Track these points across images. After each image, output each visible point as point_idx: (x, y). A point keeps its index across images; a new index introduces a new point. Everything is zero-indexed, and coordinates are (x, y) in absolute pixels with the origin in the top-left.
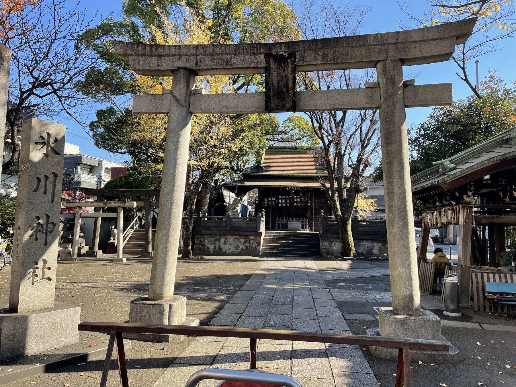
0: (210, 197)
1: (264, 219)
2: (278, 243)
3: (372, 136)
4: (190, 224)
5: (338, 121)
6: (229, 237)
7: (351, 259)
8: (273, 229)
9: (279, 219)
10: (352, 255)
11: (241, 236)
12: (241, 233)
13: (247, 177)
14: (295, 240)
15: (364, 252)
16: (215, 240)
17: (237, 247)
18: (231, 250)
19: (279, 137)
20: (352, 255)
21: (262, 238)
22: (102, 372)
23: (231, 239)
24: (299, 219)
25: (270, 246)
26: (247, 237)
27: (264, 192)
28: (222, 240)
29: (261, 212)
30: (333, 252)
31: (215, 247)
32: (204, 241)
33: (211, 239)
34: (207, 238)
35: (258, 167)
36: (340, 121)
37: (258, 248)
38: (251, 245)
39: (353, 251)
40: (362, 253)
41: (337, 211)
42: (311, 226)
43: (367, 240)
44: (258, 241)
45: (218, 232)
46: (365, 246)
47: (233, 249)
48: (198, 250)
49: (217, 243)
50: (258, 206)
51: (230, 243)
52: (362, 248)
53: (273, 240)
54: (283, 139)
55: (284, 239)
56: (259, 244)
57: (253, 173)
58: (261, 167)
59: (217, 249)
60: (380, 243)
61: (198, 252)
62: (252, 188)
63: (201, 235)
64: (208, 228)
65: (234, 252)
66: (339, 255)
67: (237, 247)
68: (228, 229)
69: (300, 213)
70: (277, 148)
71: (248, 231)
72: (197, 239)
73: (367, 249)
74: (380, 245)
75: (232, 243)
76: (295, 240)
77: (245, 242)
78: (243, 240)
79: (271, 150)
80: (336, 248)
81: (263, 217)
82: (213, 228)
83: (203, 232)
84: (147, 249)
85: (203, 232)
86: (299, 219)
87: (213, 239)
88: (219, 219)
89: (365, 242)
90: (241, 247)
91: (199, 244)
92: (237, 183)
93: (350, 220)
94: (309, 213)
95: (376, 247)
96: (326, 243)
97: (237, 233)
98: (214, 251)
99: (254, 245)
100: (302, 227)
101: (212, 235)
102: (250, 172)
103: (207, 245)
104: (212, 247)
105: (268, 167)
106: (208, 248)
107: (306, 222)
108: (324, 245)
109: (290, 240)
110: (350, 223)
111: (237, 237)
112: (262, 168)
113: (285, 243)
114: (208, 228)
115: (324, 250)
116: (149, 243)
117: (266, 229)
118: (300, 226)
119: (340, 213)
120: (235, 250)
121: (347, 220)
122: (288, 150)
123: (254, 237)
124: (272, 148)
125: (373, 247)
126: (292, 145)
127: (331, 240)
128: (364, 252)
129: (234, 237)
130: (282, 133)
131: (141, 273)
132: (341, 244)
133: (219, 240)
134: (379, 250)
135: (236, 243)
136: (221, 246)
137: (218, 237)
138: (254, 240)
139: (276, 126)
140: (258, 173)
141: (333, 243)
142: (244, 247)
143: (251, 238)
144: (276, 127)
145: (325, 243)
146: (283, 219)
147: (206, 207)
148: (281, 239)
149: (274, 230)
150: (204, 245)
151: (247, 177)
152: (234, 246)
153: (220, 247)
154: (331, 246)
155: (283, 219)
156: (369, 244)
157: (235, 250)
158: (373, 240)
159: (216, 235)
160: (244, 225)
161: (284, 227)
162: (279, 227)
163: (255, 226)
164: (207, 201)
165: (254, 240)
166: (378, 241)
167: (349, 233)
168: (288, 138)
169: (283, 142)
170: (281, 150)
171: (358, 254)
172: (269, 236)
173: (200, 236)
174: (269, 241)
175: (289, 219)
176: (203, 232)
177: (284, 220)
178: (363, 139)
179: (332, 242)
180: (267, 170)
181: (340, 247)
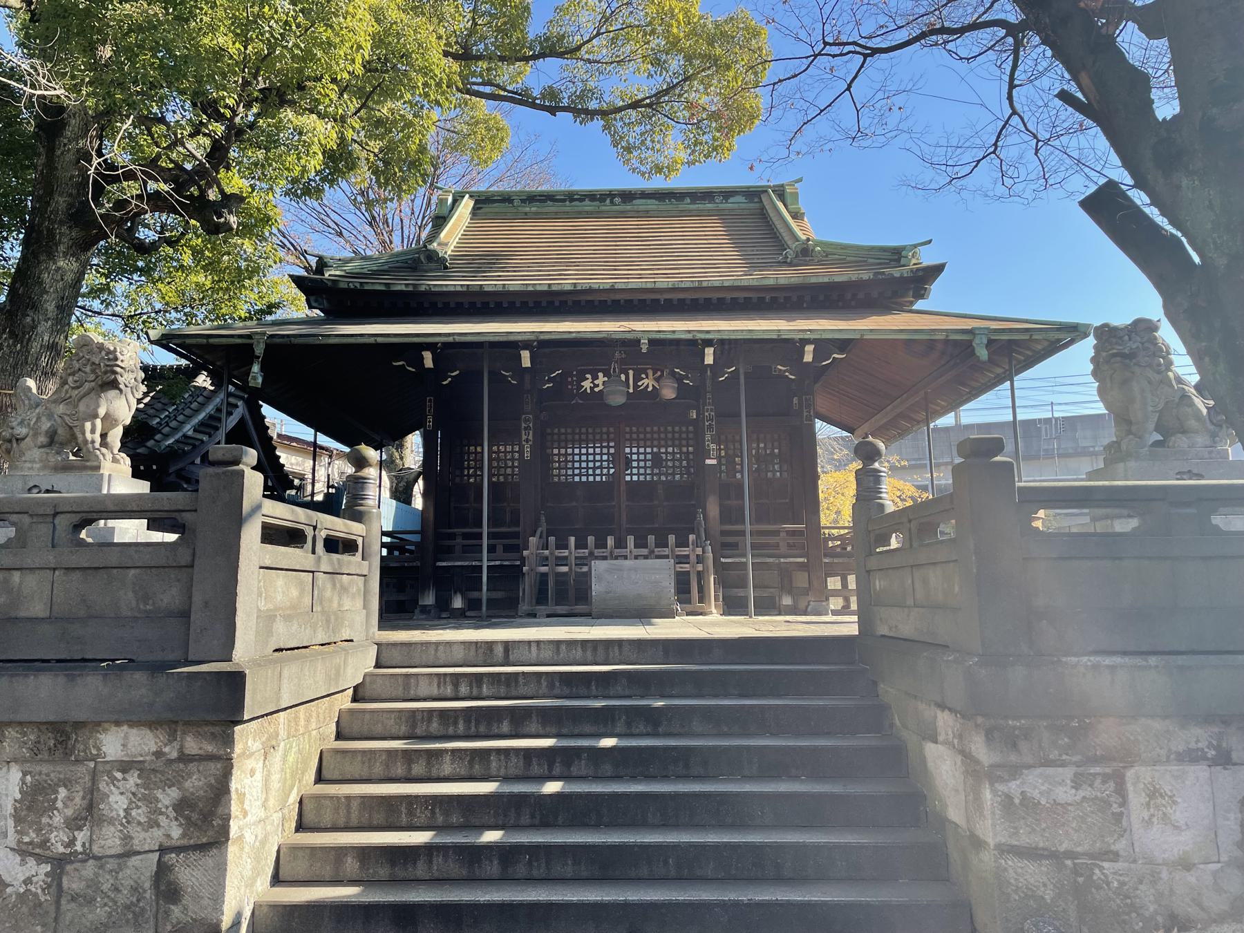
2: (477, 765)
22: (819, 424)
24: (662, 543)
25: (390, 813)
37: (188, 874)
38: (110, 840)
54: (551, 93)
56: (207, 822)
86: (662, 543)
94: (713, 509)
100: (683, 587)
107: (700, 559)
115: (1032, 875)
118: (669, 586)
122: (588, 206)
130: (552, 48)
131: (783, 534)
143: (113, 744)
145: (1034, 784)
146: (682, 543)
161: (571, 599)
170: (551, 207)
175: (601, 544)
177: (571, 550)
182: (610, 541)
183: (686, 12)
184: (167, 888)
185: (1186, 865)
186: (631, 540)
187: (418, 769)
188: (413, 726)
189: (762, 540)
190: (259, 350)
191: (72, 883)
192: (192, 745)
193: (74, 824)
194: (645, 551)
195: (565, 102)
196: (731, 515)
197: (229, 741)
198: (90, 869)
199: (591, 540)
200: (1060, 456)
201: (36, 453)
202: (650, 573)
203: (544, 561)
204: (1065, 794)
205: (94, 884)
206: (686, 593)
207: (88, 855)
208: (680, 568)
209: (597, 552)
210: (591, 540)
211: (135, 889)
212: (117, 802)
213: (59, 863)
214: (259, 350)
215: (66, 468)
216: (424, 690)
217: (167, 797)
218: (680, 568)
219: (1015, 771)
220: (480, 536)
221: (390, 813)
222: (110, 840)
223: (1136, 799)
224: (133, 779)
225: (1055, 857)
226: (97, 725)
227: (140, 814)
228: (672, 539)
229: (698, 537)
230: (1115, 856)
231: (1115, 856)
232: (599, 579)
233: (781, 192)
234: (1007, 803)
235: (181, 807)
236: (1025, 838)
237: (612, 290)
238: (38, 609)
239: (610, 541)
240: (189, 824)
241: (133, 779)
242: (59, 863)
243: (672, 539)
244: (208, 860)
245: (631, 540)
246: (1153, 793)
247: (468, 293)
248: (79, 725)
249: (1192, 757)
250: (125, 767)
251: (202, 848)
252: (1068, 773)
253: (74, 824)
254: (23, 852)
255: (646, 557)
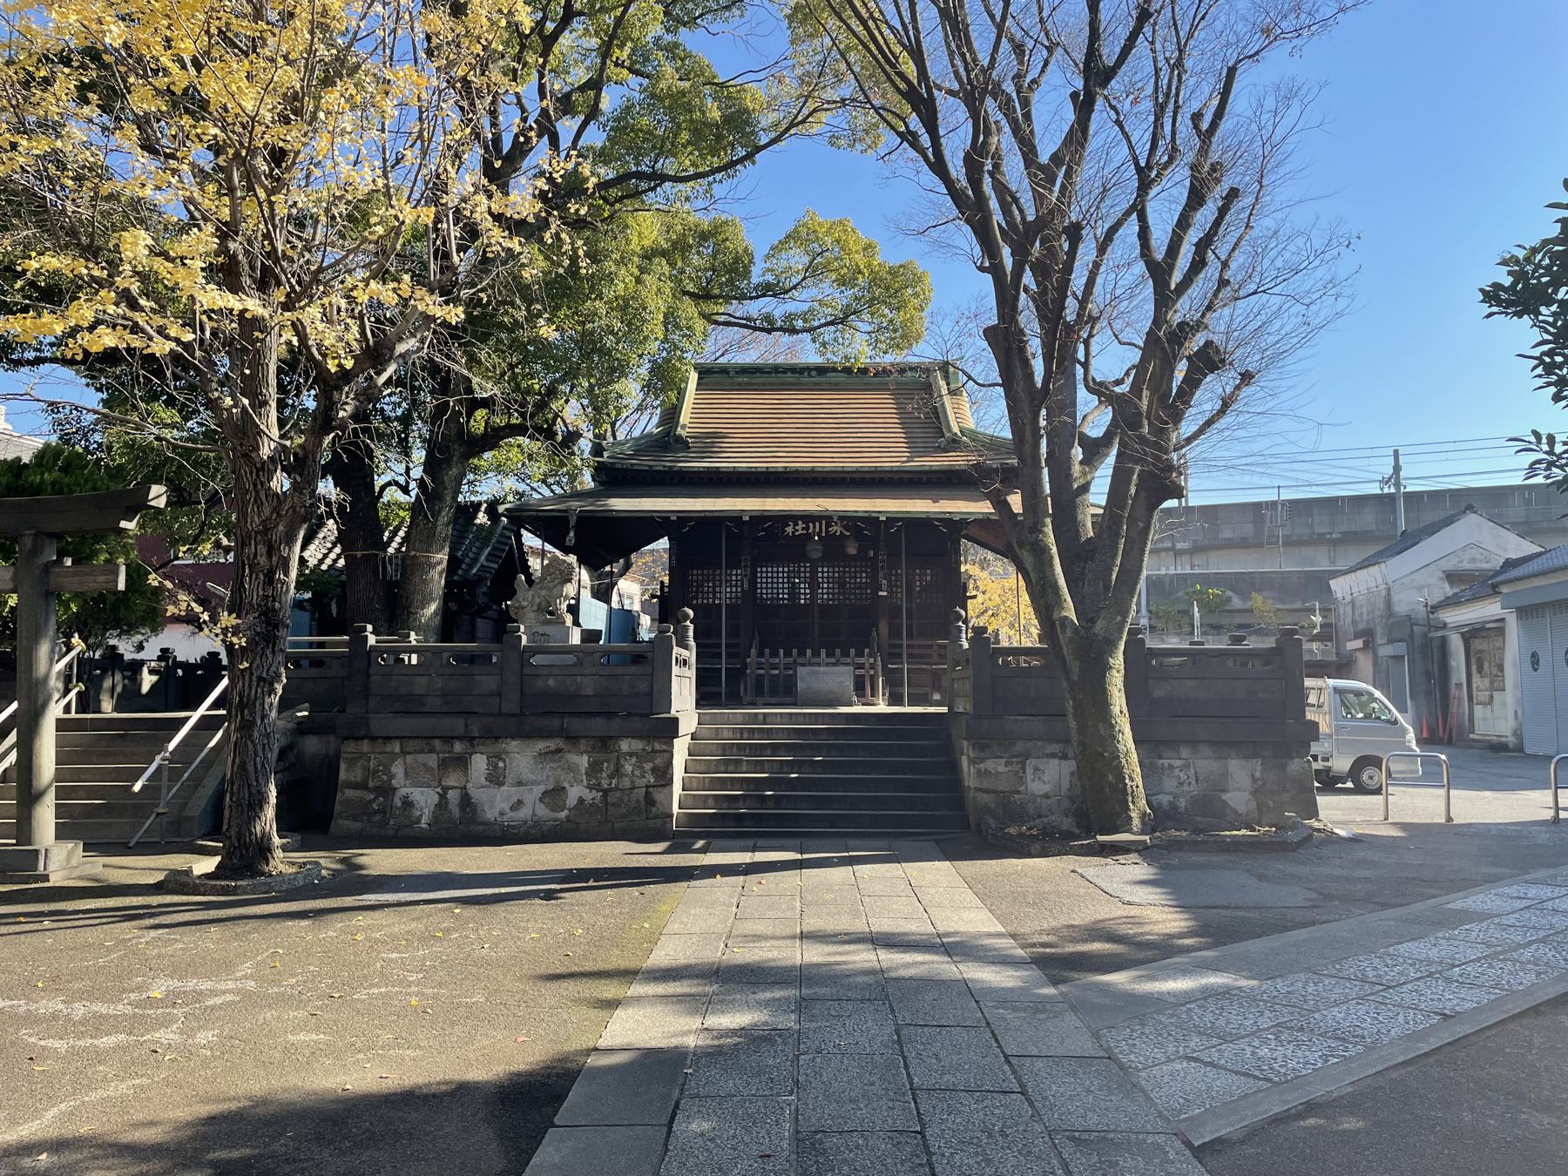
0: (454, 563)
1: (691, 655)
2: (759, 766)
3: (1217, 223)
4: (268, 683)
5: (1044, 158)
6: (514, 745)
7: (1142, 850)
8: (734, 700)
9: (761, 654)
10: (1136, 823)
11: (572, 739)
12: (575, 724)
13: (614, 477)
14: (840, 749)
15: (1182, 803)
16: (445, 764)
17: (554, 795)
18: (524, 813)
19: (754, 308)
20: (1136, 823)
21: (681, 749)
23: (522, 758)
25: (722, 784)
26: (604, 743)
27: (697, 543)
28: (479, 763)
29: (679, 622)
30: (1031, 809)
31: (443, 796)
32: (387, 771)
33: (421, 758)
34: (404, 753)
35: (667, 439)
36: (1056, 158)
37: (658, 796)
39: (1138, 807)
40: (1174, 806)
41: (1059, 602)
42: (893, 682)
43: (1194, 743)
44: (659, 761)
45: (458, 724)
46: (1189, 771)
47: (533, 808)
48: (354, 817)
49: (452, 779)
50: (666, 607)
51: (519, 776)
52: (1169, 784)
53: (731, 756)
55: (789, 749)
57: (645, 462)
58: (679, 439)
59: (456, 811)
60: (1254, 755)
61: (356, 825)
62: (649, 527)
63: (373, 739)
64: (409, 706)
65: (537, 823)
66: (1067, 823)
67: (554, 795)
68: (511, 704)
69: (844, 631)
70: (745, 370)
71: (609, 715)
72: (352, 762)
73: (1192, 789)
74: (1257, 765)
75: (527, 775)
76: (840, 749)
77: (594, 769)
78: (583, 761)
79: (713, 376)
80: (1046, 788)
81: (686, 647)
82: (433, 703)
83: (379, 724)
84: (24, 830)
85: (381, 723)
86: (846, 654)
87: (432, 760)
88: (461, 657)
89: (1185, 752)
90: (575, 792)
91: (362, 786)
92: (575, 504)
93: (1122, 647)
94: (884, 628)
95: (1240, 781)
96: (997, 766)
97: (555, 722)
98: (435, 821)
99: (641, 782)
100: (859, 687)
101: (426, 740)
102: (631, 457)
103: (405, 788)
104: (424, 799)
105: (709, 442)
106: (408, 804)
107: (872, 667)
108: (978, 772)
109: (817, 749)
110: (1118, 661)
111: (552, 744)
112: (682, 444)
113: (792, 766)
114: (409, 706)
115: (985, 798)
116: (39, 796)
117: (705, 697)
119: (1070, 612)
120: (543, 811)
121: (1111, 645)
122: (790, 377)
123: (638, 745)
124: (724, 370)
125: (1225, 775)
126: (807, 352)
127: (1019, 747)
128: (1182, 803)
129: (541, 745)
130: (767, 290)
132: (1070, 766)
133: (462, 762)
134: (1254, 793)
135: (547, 776)
136: (472, 791)
137: (458, 747)
138: (641, 757)
139: (737, 259)
140: (666, 462)
141: (1030, 764)
142: (589, 796)
143: (625, 746)
144: (738, 267)
145: (990, 765)
146: (860, 654)
147: (433, 607)
148: (775, 749)
149: (740, 705)
150: (387, 791)
151: (614, 477)
152: (538, 791)
153: (466, 800)
154: (1022, 780)
155: (775, 654)
156: (1205, 763)
157: (543, 811)
158: (1224, 745)
159: (448, 739)
160: (588, 686)
161: (784, 691)
162: (759, 690)
163: (643, 687)
164: (437, 579)
165: (641, 757)
166: (1248, 748)
167: (1116, 710)
168: (790, 317)
169: (769, 331)
170: (760, 379)
171: (1158, 819)
172: (717, 734)
173: (365, 746)
174: (716, 756)
175: (802, 654)
176: (381, 723)
177: (781, 658)
178: (1159, 255)
179: (1026, 755)
180: (705, 452)
181: (1066, 783)
182: (809, 652)
183: (869, 265)
184: (650, 801)
185: (1047, 796)
186: (823, 652)
187: (730, 768)
188: (724, 749)
189: (914, 651)
190: (573, 522)
191: (612, 799)
192: (657, 746)
193: (611, 777)
194: (833, 660)
195: (779, 324)
196: (895, 632)
197: (672, 745)
198: (618, 794)
199: (795, 651)
200: (1286, 544)
201: (532, 615)
202: (838, 677)
203: (760, 666)
204: (1001, 769)
205: (621, 799)
206: (862, 688)
207: (617, 789)
208: (858, 672)
209: (800, 660)
210: (795, 651)
211: (638, 801)
212: (628, 768)
213: (606, 792)
214: (573, 522)
215: (548, 622)
216: (726, 734)
217: (648, 766)
218: (858, 672)
219: (983, 760)
220: (720, 645)
221: (722, 784)
222: (626, 783)
223: (1029, 771)
224: (634, 760)
225: (996, 792)
226: (619, 737)
227: (637, 773)
228: (853, 651)
229: (872, 649)
230: (1019, 792)
231: (1019, 792)
232: (803, 679)
233: (945, 367)
234: (979, 772)
235: (653, 770)
236: (985, 785)
237: (813, 470)
238: (590, 692)
239: (809, 652)
240: (657, 777)
241: (634, 760)
242: (606, 792)
243: (853, 651)
244: (666, 790)
245: (823, 652)
246: (1036, 769)
247: (709, 471)
248: (611, 738)
249: (1053, 755)
250: (631, 754)
251: (663, 786)
252: (1003, 761)
253: (611, 777)
254: (590, 788)
255: (833, 665)
